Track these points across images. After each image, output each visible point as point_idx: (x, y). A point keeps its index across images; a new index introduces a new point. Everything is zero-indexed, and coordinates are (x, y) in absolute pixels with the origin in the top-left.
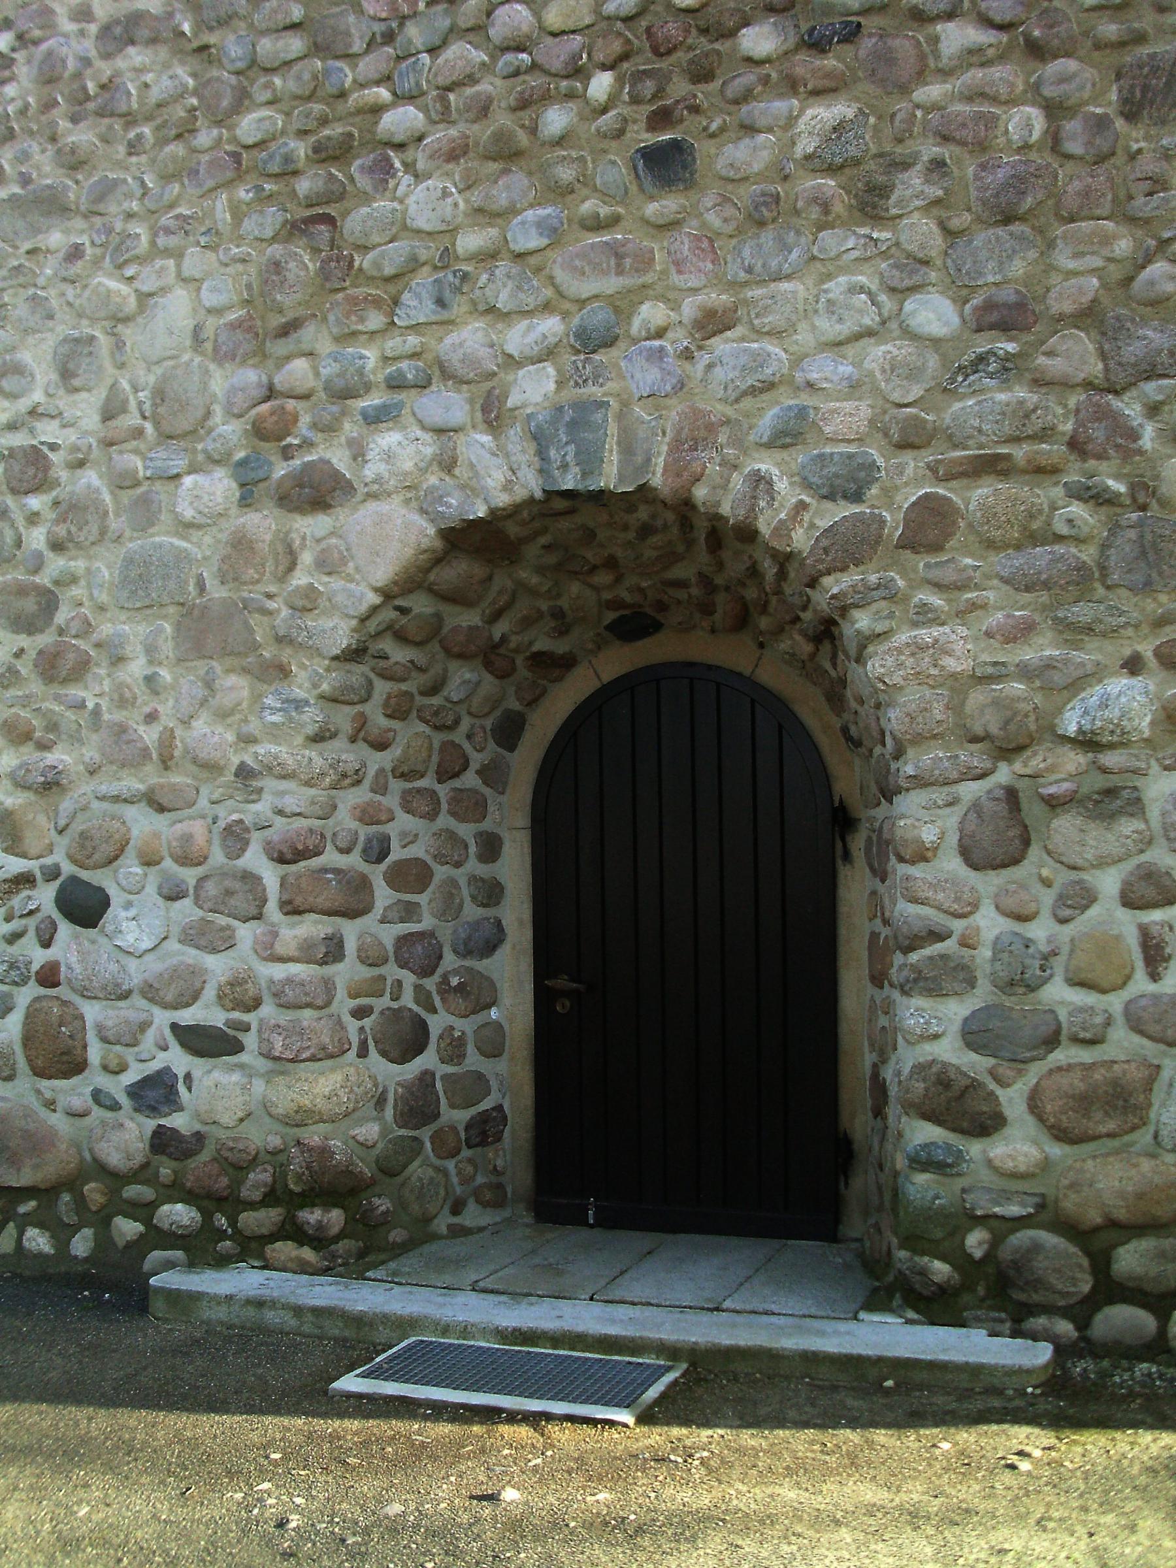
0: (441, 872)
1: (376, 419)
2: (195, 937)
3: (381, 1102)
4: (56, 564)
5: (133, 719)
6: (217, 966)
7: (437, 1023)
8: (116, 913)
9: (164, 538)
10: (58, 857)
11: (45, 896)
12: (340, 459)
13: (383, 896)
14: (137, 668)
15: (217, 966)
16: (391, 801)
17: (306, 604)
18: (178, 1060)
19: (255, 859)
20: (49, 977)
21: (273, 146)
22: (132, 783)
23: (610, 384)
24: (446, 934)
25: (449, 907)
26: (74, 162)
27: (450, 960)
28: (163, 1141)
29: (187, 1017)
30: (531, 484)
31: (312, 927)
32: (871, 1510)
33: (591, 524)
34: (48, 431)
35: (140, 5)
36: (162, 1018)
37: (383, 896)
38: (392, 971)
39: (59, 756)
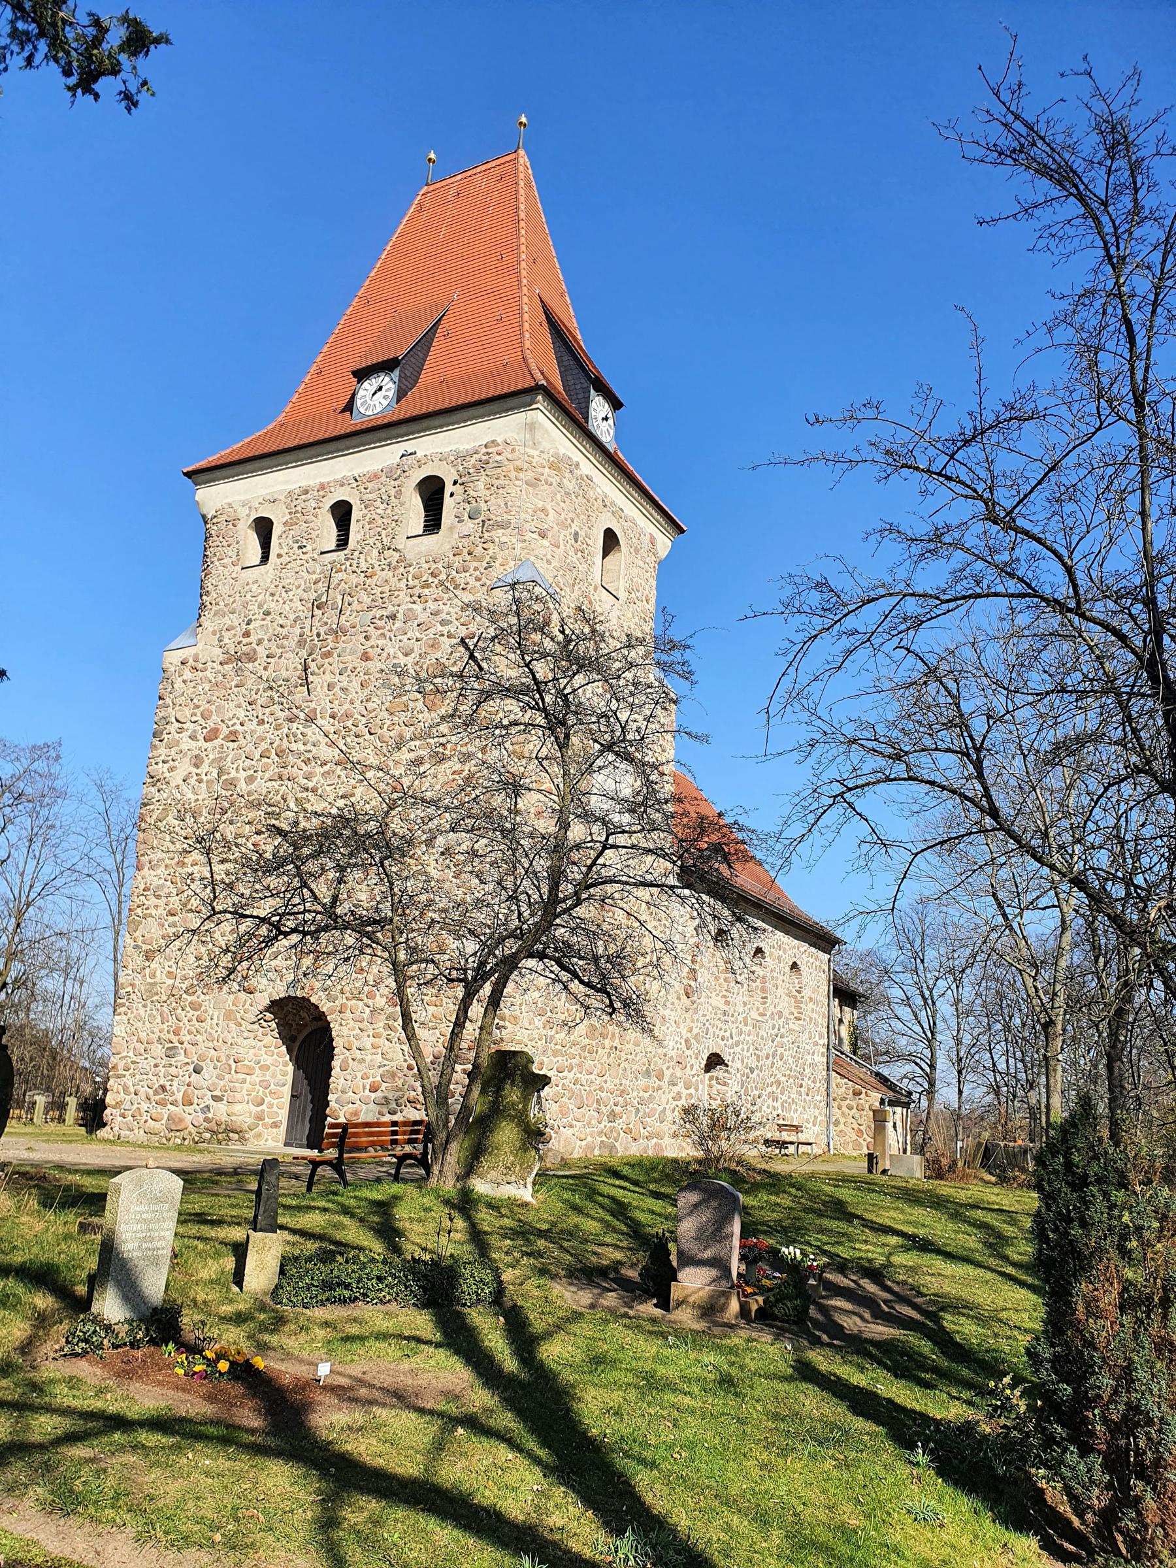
0: (272, 1068)
5: (213, 1032)
7: (267, 1100)
10: (195, 1059)
11: (191, 1068)
13: (258, 1071)
15: (222, 1083)
16: (263, 1052)
18: (211, 1102)
19: (231, 1062)
21: (544, 774)
22: (211, 1045)
24: (272, 1081)
25: (274, 1075)
27: (272, 1086)
28: (206, 1120)
29: (214, 1093)
33: (279, 991)
35: (1161, 169)
36: (210, 1094)
37: (258, 1071)
38: (257, 1087)
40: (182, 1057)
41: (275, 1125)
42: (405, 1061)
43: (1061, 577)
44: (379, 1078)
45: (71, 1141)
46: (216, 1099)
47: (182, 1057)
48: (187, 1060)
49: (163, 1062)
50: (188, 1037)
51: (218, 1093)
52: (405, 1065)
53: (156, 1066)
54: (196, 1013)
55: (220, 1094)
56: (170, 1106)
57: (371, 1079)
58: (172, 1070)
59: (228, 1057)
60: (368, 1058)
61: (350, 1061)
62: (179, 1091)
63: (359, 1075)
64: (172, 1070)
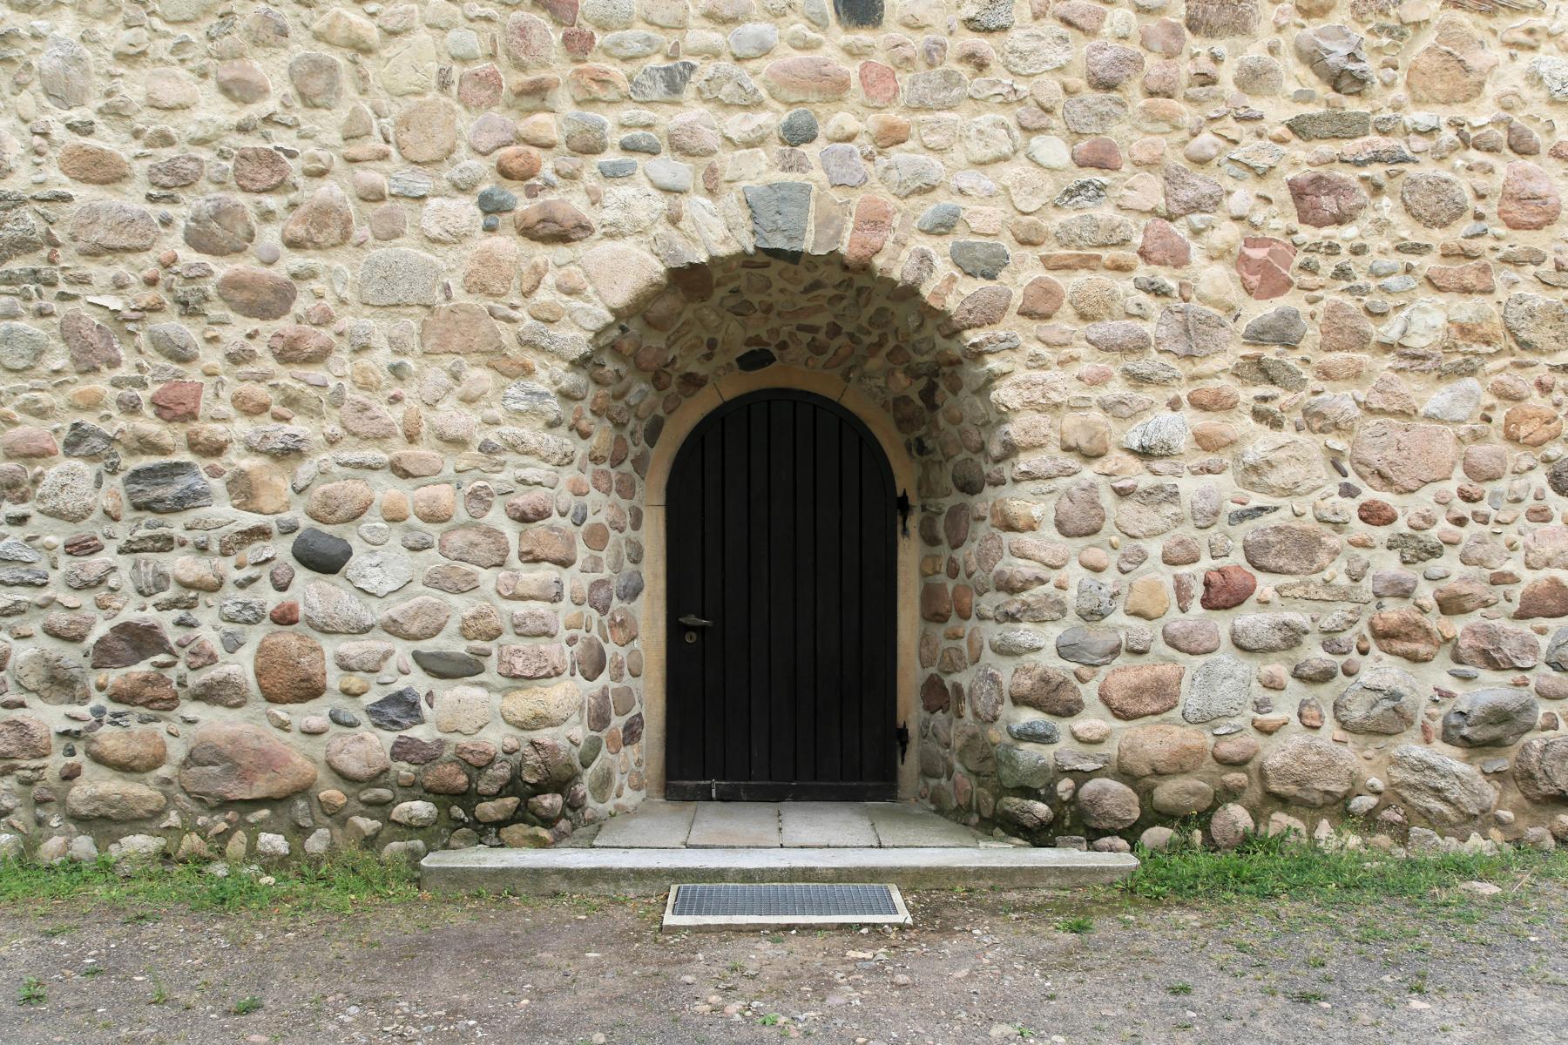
1: (612, 174)
3: (755, 359)
4: (294, 261)
6: (462, 606)
8: (359, 560)
11: (281, 549)
14: (382, 356)
15: (462, 606)
18: (419, 682)
19: (496, 517)
20: (285, 618)
34: (283, 139)
39: (299, 426)
40: (224, 512)
41: (632, 733)
42: (1348, 491)
43: (1040, 155)
44: (1237, 558)
45: (92, 553)
46: (443, 668)
47: (224, 512)
48: (250, 520)
49: (122, 532)
50: (242, 427)
51: (451, 643)
52: (1351, 507)
53: (81, 548)
54: (267, 328)
55: (461, 647)
56: (191, 709)
57: (1206, 563)
58: (181, 564)
59: (479, 498)
60: (1189, 486)
61: (1107, 499)
62: (233, 644)
63: (1154, 548)
64: (181, 564)
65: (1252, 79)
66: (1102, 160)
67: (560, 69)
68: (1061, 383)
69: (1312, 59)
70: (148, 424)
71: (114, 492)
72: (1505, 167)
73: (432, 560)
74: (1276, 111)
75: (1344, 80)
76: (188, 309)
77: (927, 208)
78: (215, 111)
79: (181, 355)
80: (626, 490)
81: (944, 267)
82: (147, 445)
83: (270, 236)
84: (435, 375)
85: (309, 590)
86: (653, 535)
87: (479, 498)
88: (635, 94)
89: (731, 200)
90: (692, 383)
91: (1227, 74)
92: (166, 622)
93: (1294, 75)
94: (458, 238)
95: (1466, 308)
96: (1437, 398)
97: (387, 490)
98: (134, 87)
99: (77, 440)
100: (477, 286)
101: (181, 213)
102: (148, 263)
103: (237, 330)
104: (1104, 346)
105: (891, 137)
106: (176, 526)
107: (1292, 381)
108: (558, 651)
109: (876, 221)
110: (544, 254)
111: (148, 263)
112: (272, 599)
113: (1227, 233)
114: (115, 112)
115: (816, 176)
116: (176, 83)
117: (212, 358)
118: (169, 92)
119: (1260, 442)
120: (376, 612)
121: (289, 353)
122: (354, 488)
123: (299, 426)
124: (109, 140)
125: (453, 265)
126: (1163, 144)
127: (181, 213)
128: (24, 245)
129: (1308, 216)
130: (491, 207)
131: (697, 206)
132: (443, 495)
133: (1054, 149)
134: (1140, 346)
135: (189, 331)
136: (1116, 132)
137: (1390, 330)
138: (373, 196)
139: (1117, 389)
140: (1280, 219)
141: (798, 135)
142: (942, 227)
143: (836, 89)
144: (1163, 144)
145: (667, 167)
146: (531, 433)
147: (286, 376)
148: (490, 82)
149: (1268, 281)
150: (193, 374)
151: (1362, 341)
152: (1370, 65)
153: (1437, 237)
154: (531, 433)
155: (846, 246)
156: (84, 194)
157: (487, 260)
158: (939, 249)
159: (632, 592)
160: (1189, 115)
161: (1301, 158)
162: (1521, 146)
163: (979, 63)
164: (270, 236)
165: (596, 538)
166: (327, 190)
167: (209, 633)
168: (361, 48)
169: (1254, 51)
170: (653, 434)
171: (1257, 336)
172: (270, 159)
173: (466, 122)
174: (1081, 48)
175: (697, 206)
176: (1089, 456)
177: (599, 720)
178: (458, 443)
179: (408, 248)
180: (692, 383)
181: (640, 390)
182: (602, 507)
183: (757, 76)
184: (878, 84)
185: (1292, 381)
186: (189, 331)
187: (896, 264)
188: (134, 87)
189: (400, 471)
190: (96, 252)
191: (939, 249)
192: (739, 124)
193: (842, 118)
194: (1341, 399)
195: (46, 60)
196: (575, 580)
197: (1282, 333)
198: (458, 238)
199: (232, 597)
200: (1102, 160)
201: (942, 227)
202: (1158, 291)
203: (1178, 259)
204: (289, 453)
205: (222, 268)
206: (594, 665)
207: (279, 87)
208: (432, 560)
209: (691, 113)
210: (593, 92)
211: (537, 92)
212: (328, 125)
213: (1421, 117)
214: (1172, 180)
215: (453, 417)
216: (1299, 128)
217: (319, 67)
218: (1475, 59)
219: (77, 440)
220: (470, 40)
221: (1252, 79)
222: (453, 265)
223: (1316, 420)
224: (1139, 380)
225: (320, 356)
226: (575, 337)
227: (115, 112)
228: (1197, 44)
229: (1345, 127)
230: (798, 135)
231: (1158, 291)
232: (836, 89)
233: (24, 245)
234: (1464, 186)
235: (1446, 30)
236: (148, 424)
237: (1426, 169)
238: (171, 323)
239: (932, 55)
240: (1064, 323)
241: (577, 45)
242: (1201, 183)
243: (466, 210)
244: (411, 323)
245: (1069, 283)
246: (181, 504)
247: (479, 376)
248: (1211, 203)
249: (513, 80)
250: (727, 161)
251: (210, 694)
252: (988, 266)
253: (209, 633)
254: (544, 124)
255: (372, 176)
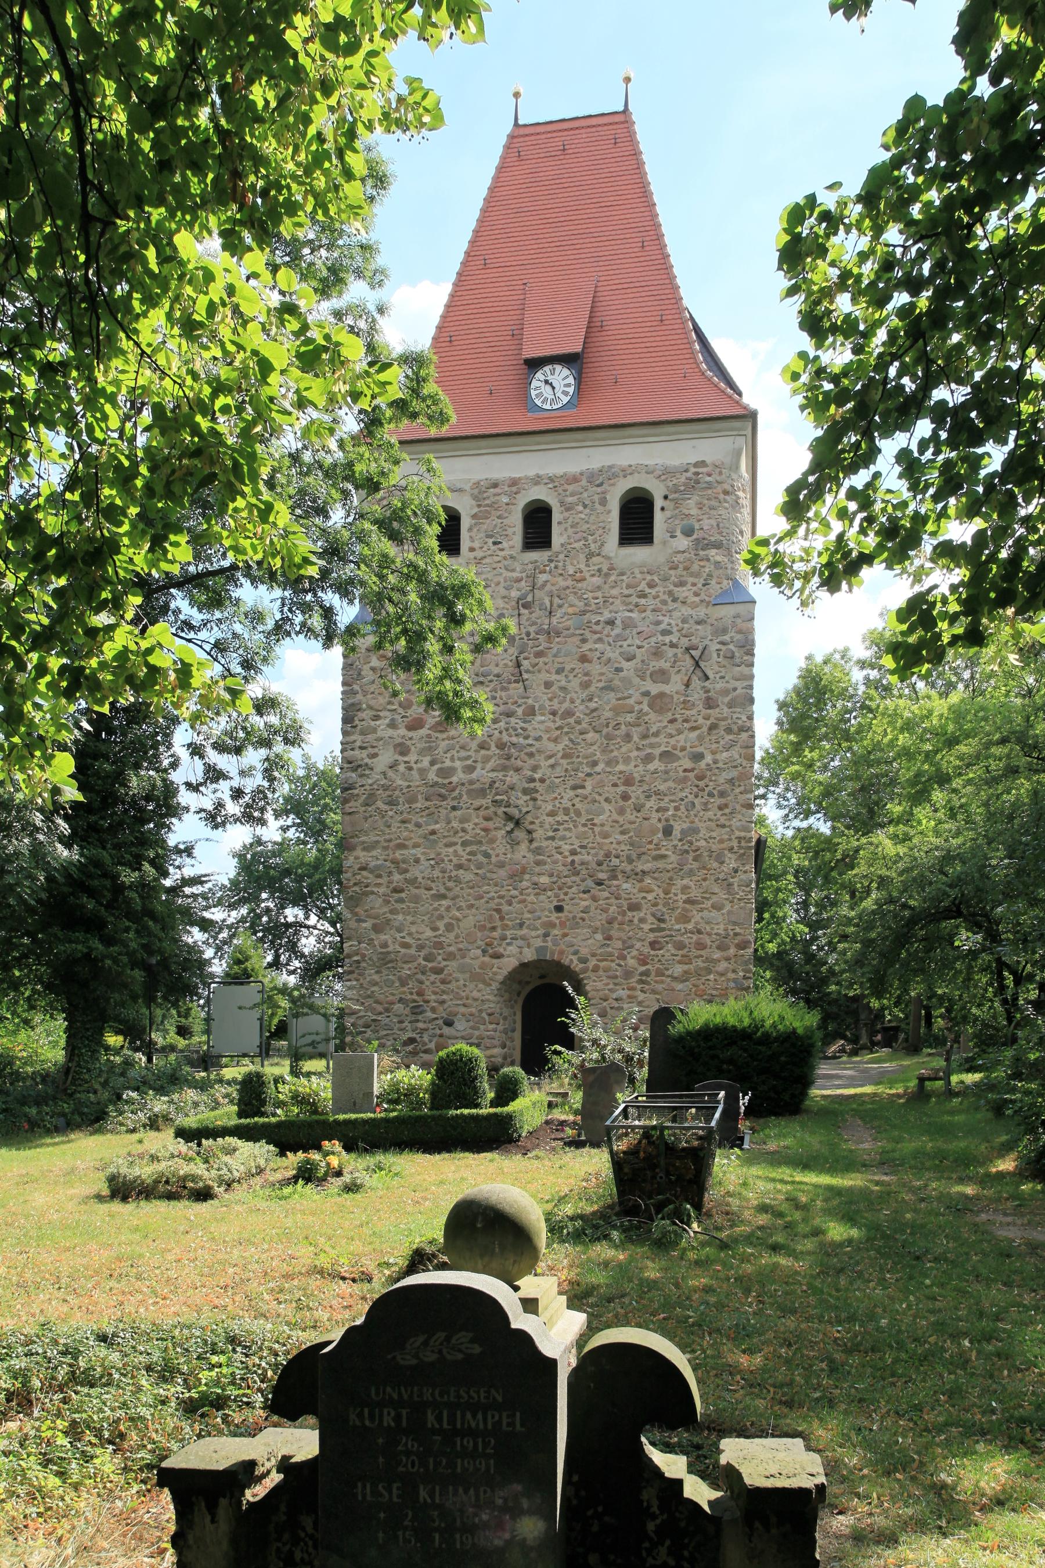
1: (508, 944)
2: (472, 1028)
3: (542, 977)
4: (445, 963)
6: (477, 1033)
8: (456, 1024)
9: (467, 960)
11: (440, 1022)
12: (501, 950)
14: (462, 982)
15: (477, 1033)
17: (495, 974)
19: (484, 1015)
20: (441, 1036)
23: (683, 480)
26: (449, 889)
30: (535, 957)
31: (494, 1026)
32: (129, 338)
34: (443, 939)
39: (445, 997)
50: (433, 997)
54: (439, 977)
58: (421, 1025)
64: (421, 1025)
65: (642, 920)
66: (609, 938)
67: (498, 923)
68: (599, 985)
69: (653, 915)
70: (415, 997)
71: (407, 1011)
72: (695, 937)
73: (471, 1023)
74: (646, 927)
75: (661, 920)
76: (423, 973)
77: (572, 950)
78: (429, 933)
79: (422, 983)
80: (512, 1007)
81: (575, 962)
82: (415, 1001)
83: (440, 958)
84: (472, 986)
85: (446, 1030)
86: (519, 1017)
87: (481, 1011)
88: (513, 928)
89: (533, 949)
90: (528, 983)
91: (636, 921)
92: (417, 1037)
93: (650, 919)
94: (477, 958)
95: (686, 967)
96: (680, 986)
97: (462, 1009)
98: (413, 929)
99: (401, 1000)
100: (481, 968)
101: (422, 954)
102: (415, 964)
103: (433, 977)
104: (609, 977)
105: (565, 935)
106: (420, 1017)
107: (648, 983)
108: (496, 1042)
109: (562, 952)
110: (495, 961)
111: (415, 964)
112: (438, 1032)
113: (635, 953)
114: (410, 934)
115: (550, 944)
116: (422, 927)
117: (427, 983)
118: (421, 930)
119: (641, 996)
120: (459, 1034)
121: (443, 982)
122: (456, 1009)
123: (445, 997)
124: (408, 940)
125: (476, 964)
126: (622, 935)
127: (422, 954)
128: (391, 961)
129: (653, 949)
130: (484, 951)
131: (526, 950)
132: (473, 1010)
133: (599, 937)
134: (616, 977)
135: (423, 978)
136: (612, 933)
137: (669, 972)
138: (460, 950)
139: (611, 986)
140: (647, 950)
141: (546, 935)
142: (576, 953)
143: (553, 925)
144: (622, 935)
145: (520, 942)
146: (491, 997)
147: (442, 987)
148: (484, 926)
149: (644, 962)
150: (221, 309)
151: (663, 975)
152: (667, 917)
153: (681, 952)
154: (491, 997)
155: (556, 957)
156: (403, 950)
157: (483, 963)
158: (574, 958)
159: (513, 1031)
160: (627, 928)
161: (652, 936)
162: (699, 932)
163: (583, 919)
164: (440, 958)
165: (505, 1018)
166: (452, 949)
167: (426, 1039)
168: (458, 920)
169: (642, 915)
170: (519, 994)
171: (641, 974)
172: (440, 943)
173: (479, 934)
174: (605, 915)
175: (526, 950)
176: (606, 1000)
177: (505, 1058)
178: (476, 1000)
179: (467, 960)
180: (528, 983)
181: (516, 986)
182: (506, 1012)
183: (538, 923)
184: (563, 924)
185: (648, 983)
186: (423, 978)
187: (566, 961)
188: (413, 929)
189: (464, 1005)
190: (405, 962)
191: (574, 958)
192: (534, 933)
193: (556, 932)
194: (659, 987)
195: (397, 924)
196: (500, 1027)
197: (646, 973)
198: (477, 958)
199: (431, 1032)
200: (609, 938)
201: (576, 953)
202: (619, 965)
203: (624, 958)
204: (443, 1002)
205: (430, 965)
206: (504, 1046)
207: (442, 928)
208: (471, 1023)
209: (524, 931)
210: (505, 927)
211: (494, 928)
212: (452, 936)
213: (677, 927)
214: (624, 942)
215: (475, 994)
216: (651, 930)
217: (450, 924)
218: (690, 914)
219: (401, 1000)
220: (481, 918)
221: (642, 920)
222: (476, 964)
223: (654, 992)
224: (615, 984)
225: (449, 982)
226: (500, 978)
227: (410, 934)
228: (630, 914)
229: (660, 930)
230: (546, 935)
231: (619, 965)
232: (553, 925)
233: (391, 961)
234: (687, 941)
235: (684, 909)
236: (415, 997)
237: (679, 938)
238: (420, 976)
239: (574, 918)
240: (601, 973)
241: (502, 918)
242: (629, 943)
243: (479, 952)
244: (468, 975)
245: (602, 964)
246: (421, 1013)
247: (481, 986)
248: (632, 947)
249: (489, 926)
250: (532, 941)
251: (426, 1052)
252: (583, 960)
253: (426, 1039)
254: (495, 934)
255: (461, 946)
